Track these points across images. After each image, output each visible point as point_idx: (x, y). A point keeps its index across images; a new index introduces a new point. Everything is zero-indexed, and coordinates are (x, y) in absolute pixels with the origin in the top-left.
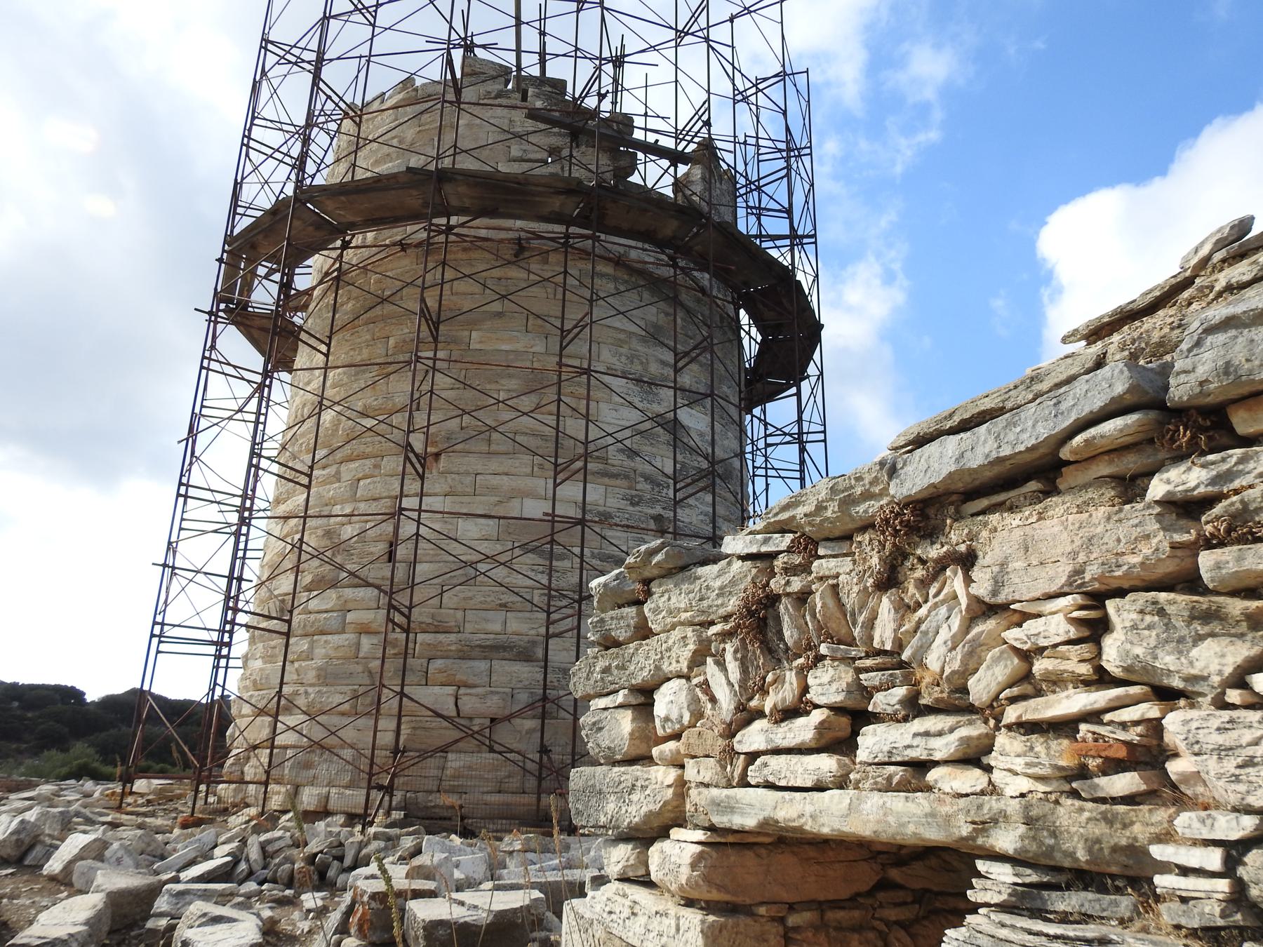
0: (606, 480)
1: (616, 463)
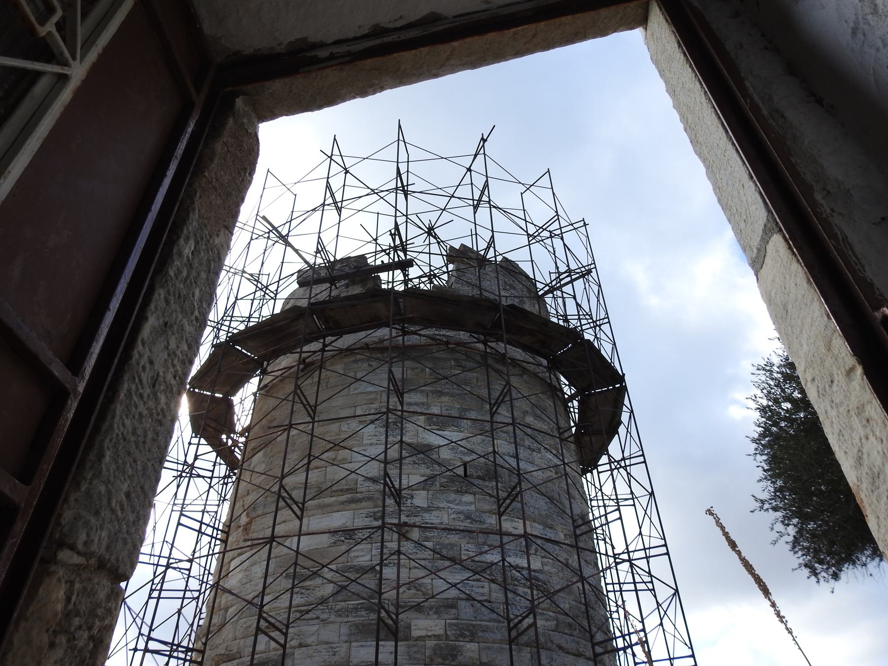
0: (353, 506)
1: (363, 490)
